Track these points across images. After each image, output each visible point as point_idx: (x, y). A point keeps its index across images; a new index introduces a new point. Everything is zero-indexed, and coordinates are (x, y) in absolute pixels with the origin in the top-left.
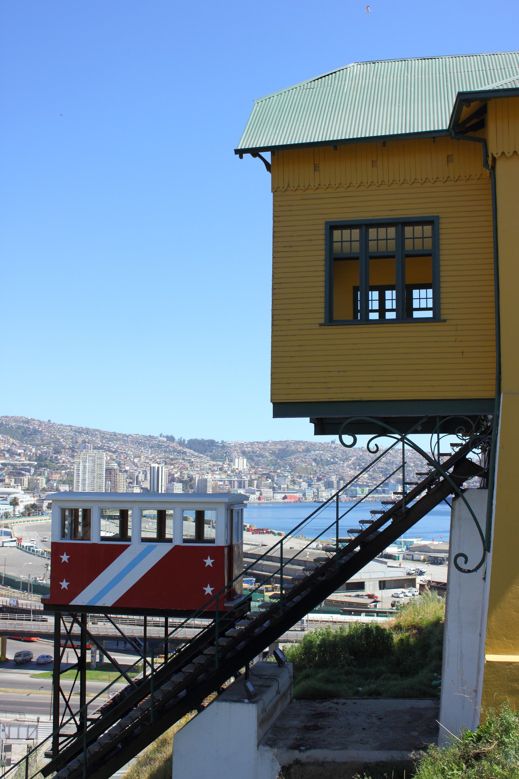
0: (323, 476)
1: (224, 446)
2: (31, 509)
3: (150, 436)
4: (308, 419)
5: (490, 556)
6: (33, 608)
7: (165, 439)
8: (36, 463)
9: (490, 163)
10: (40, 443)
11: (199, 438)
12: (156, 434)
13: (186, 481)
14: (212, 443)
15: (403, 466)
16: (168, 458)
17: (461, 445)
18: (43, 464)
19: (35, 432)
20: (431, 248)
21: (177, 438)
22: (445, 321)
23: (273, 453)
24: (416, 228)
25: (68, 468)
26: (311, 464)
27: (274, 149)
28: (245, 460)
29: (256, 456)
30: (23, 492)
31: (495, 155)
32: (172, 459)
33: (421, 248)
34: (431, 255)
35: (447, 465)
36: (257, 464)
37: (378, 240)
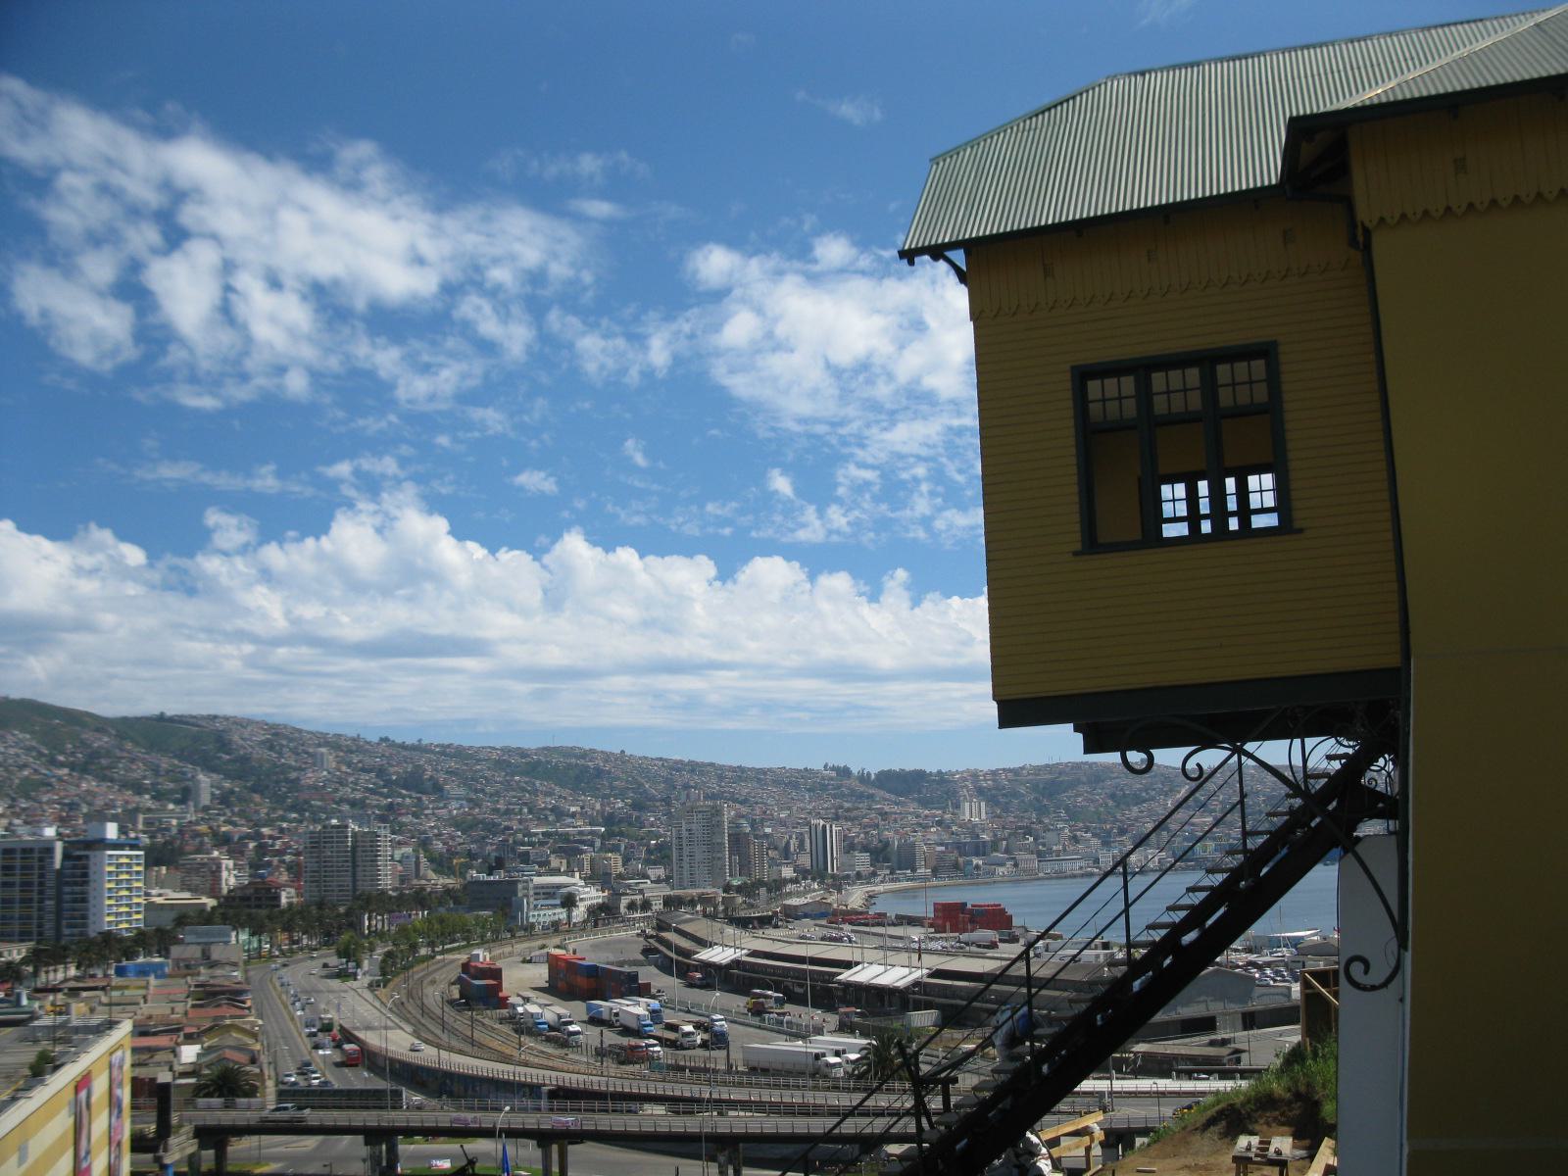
0: (1130, 825)
1: (942, 779)
2: (598, 912)
3: (806, 769)
4: (1071, 726)
5: (1408, 956)
6: (611, 1089)
7: (834, 774)
8: (603, 829)
9: (1361, 239)
10: (607, 792)
11: (896, 767)
12: (818, 766)
13: (876, 848)
14: (920, 775)
15: (1241, 802)
16: (841, 807)
17: (1345, 756)
18: (616, 829)
19: (599, 773)
20: (1266, 399)
21: (855, 770)
22: (1301, 531)
23: (1035, 787)
24: (1106, 381)
25: (661, 836)
26: (1107, 805)
27: (970, 246)
28: (983, 804)
29: (1004, 795)
30: (582, 883)
31: (1367, 224)
32: (848, 810)
33: (1166, 412)
34: (1271, 410)
35: (1325, 795)
36: (1006, 810)
37: (1168, 392)
